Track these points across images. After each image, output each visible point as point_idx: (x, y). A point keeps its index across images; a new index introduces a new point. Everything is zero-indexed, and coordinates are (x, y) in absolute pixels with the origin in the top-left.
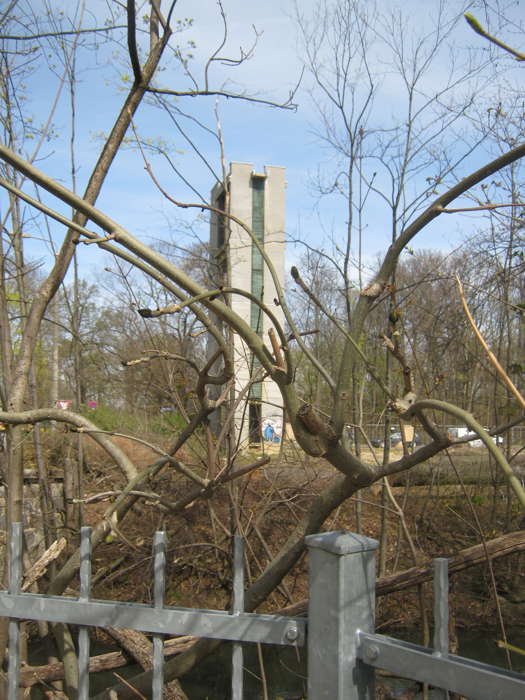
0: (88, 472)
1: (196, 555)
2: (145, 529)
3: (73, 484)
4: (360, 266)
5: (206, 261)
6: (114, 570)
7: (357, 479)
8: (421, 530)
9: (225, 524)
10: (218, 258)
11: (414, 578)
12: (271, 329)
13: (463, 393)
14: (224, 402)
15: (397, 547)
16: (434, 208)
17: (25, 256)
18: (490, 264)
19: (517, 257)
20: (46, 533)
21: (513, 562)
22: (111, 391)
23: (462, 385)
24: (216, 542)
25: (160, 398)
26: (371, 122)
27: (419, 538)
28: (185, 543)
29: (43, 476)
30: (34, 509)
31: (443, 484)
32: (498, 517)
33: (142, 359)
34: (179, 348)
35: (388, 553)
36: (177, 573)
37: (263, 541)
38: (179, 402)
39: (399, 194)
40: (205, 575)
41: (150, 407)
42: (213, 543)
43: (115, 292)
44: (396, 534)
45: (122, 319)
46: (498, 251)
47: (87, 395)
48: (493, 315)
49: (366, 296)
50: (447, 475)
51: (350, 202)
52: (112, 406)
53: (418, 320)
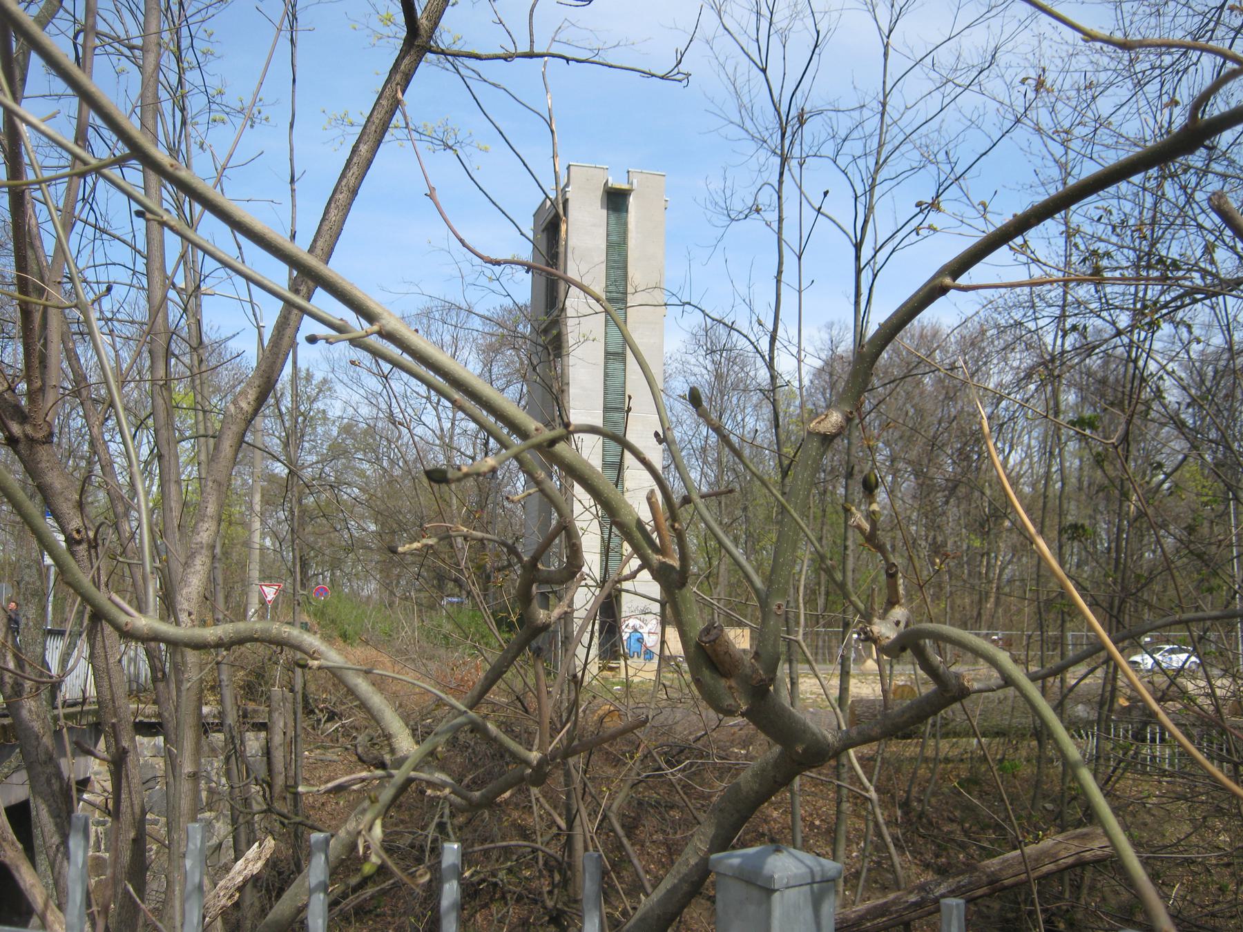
0: (312, 712)
1: (503, 863)
2: (412, 815)
3: (285, 733)
4: (799, 352)
5: (524, 337)
6: (355, 889)
7: (801, 753)
8: (908, 822)
9: (555, 808)
10: (546, 331)
11: (897, 911)
12: (652, 491)
13: (980, 573)
14: (566, 613)
15: (864, 850)
16: (937, 282)
17: (205, 328)
18: (1028, 347)
19: (1075, 335)
20: (234, 821)
21: (1073, 877)
22: (353, 566)
23: (979, 558)
24: (539, 840)
25: (441, 579)
26: (817, 94)
27: (903, 834)
28: (484, 841)
29: (231, 719)
30: (215, 779)
31: (946, 735)
32: (1045, 797)
33: (425, 541)
34: (476, 489)
35: (848, 861)
36: (469, 895)
37: (625, 841)
38: (476, 590)
39: (866, 222)
40: (519, 899)
41: (422, 595)
42: (535, 841)
43: (362, 392)
44: (863, 826)
45: (375, 440)
46: (1041, 323)
47: (311, 573)
48: (1034, 434)
49: (818, 433)
50: (953, 720)
51: (780, 240)
52: (355, 594)
53: (900, 444)
